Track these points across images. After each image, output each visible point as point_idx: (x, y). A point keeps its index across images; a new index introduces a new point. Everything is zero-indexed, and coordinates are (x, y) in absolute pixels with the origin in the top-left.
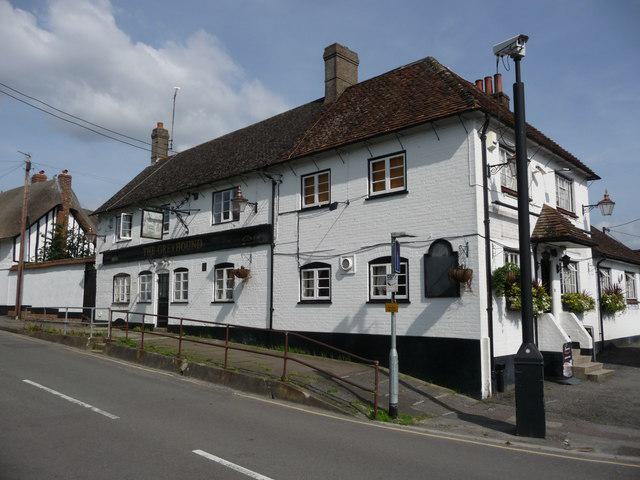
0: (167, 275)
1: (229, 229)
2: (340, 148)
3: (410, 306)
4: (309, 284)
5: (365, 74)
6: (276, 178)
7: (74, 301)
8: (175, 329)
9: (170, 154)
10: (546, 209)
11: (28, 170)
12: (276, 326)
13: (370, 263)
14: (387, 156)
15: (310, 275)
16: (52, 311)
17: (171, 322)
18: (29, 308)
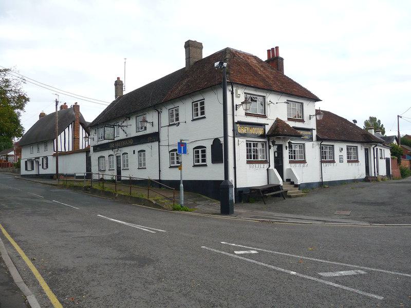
0: (120, 156)
1: (141, 134)
2: (182, 97)
3: (306, 164)
4: (173, 159)
5: (206, 53)
6: (159, 110)
7: (82, 171)
8: (125, 181)
9: (124, 93)
10: (278, 122)
11: (57, 105)
12: (163, 178)
13: (170, 152)
14: (198, 101)
15: (173, 155)
16: (73, 176)
17: (122, 178)
18: (62, 175)
